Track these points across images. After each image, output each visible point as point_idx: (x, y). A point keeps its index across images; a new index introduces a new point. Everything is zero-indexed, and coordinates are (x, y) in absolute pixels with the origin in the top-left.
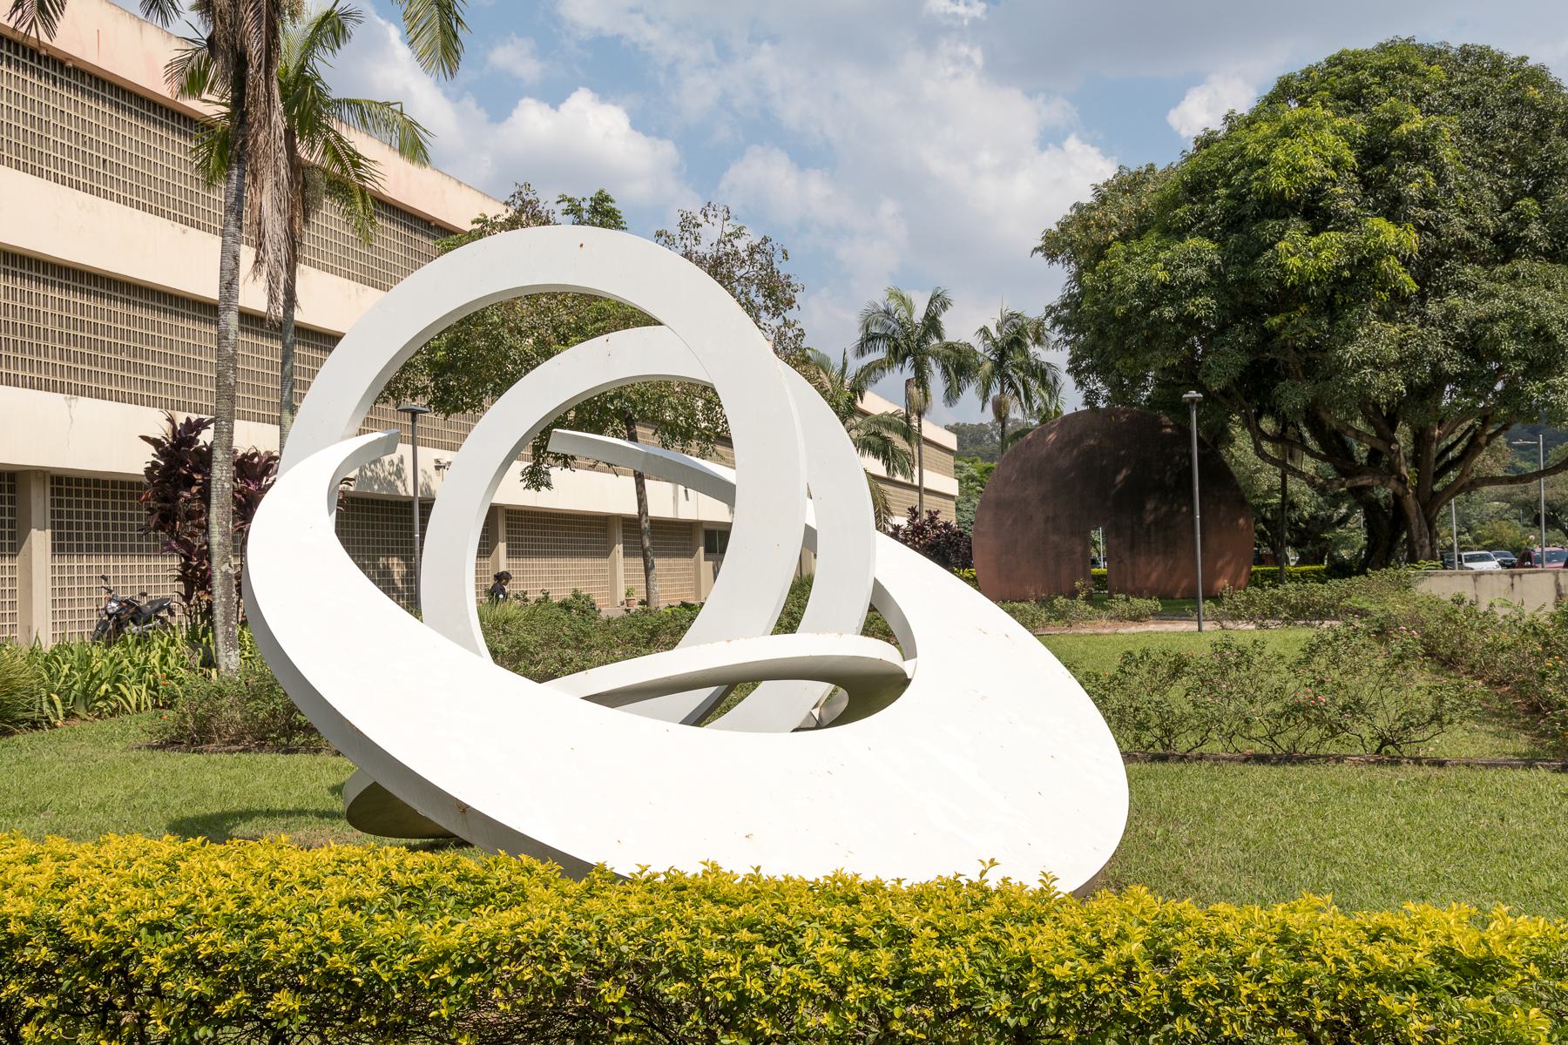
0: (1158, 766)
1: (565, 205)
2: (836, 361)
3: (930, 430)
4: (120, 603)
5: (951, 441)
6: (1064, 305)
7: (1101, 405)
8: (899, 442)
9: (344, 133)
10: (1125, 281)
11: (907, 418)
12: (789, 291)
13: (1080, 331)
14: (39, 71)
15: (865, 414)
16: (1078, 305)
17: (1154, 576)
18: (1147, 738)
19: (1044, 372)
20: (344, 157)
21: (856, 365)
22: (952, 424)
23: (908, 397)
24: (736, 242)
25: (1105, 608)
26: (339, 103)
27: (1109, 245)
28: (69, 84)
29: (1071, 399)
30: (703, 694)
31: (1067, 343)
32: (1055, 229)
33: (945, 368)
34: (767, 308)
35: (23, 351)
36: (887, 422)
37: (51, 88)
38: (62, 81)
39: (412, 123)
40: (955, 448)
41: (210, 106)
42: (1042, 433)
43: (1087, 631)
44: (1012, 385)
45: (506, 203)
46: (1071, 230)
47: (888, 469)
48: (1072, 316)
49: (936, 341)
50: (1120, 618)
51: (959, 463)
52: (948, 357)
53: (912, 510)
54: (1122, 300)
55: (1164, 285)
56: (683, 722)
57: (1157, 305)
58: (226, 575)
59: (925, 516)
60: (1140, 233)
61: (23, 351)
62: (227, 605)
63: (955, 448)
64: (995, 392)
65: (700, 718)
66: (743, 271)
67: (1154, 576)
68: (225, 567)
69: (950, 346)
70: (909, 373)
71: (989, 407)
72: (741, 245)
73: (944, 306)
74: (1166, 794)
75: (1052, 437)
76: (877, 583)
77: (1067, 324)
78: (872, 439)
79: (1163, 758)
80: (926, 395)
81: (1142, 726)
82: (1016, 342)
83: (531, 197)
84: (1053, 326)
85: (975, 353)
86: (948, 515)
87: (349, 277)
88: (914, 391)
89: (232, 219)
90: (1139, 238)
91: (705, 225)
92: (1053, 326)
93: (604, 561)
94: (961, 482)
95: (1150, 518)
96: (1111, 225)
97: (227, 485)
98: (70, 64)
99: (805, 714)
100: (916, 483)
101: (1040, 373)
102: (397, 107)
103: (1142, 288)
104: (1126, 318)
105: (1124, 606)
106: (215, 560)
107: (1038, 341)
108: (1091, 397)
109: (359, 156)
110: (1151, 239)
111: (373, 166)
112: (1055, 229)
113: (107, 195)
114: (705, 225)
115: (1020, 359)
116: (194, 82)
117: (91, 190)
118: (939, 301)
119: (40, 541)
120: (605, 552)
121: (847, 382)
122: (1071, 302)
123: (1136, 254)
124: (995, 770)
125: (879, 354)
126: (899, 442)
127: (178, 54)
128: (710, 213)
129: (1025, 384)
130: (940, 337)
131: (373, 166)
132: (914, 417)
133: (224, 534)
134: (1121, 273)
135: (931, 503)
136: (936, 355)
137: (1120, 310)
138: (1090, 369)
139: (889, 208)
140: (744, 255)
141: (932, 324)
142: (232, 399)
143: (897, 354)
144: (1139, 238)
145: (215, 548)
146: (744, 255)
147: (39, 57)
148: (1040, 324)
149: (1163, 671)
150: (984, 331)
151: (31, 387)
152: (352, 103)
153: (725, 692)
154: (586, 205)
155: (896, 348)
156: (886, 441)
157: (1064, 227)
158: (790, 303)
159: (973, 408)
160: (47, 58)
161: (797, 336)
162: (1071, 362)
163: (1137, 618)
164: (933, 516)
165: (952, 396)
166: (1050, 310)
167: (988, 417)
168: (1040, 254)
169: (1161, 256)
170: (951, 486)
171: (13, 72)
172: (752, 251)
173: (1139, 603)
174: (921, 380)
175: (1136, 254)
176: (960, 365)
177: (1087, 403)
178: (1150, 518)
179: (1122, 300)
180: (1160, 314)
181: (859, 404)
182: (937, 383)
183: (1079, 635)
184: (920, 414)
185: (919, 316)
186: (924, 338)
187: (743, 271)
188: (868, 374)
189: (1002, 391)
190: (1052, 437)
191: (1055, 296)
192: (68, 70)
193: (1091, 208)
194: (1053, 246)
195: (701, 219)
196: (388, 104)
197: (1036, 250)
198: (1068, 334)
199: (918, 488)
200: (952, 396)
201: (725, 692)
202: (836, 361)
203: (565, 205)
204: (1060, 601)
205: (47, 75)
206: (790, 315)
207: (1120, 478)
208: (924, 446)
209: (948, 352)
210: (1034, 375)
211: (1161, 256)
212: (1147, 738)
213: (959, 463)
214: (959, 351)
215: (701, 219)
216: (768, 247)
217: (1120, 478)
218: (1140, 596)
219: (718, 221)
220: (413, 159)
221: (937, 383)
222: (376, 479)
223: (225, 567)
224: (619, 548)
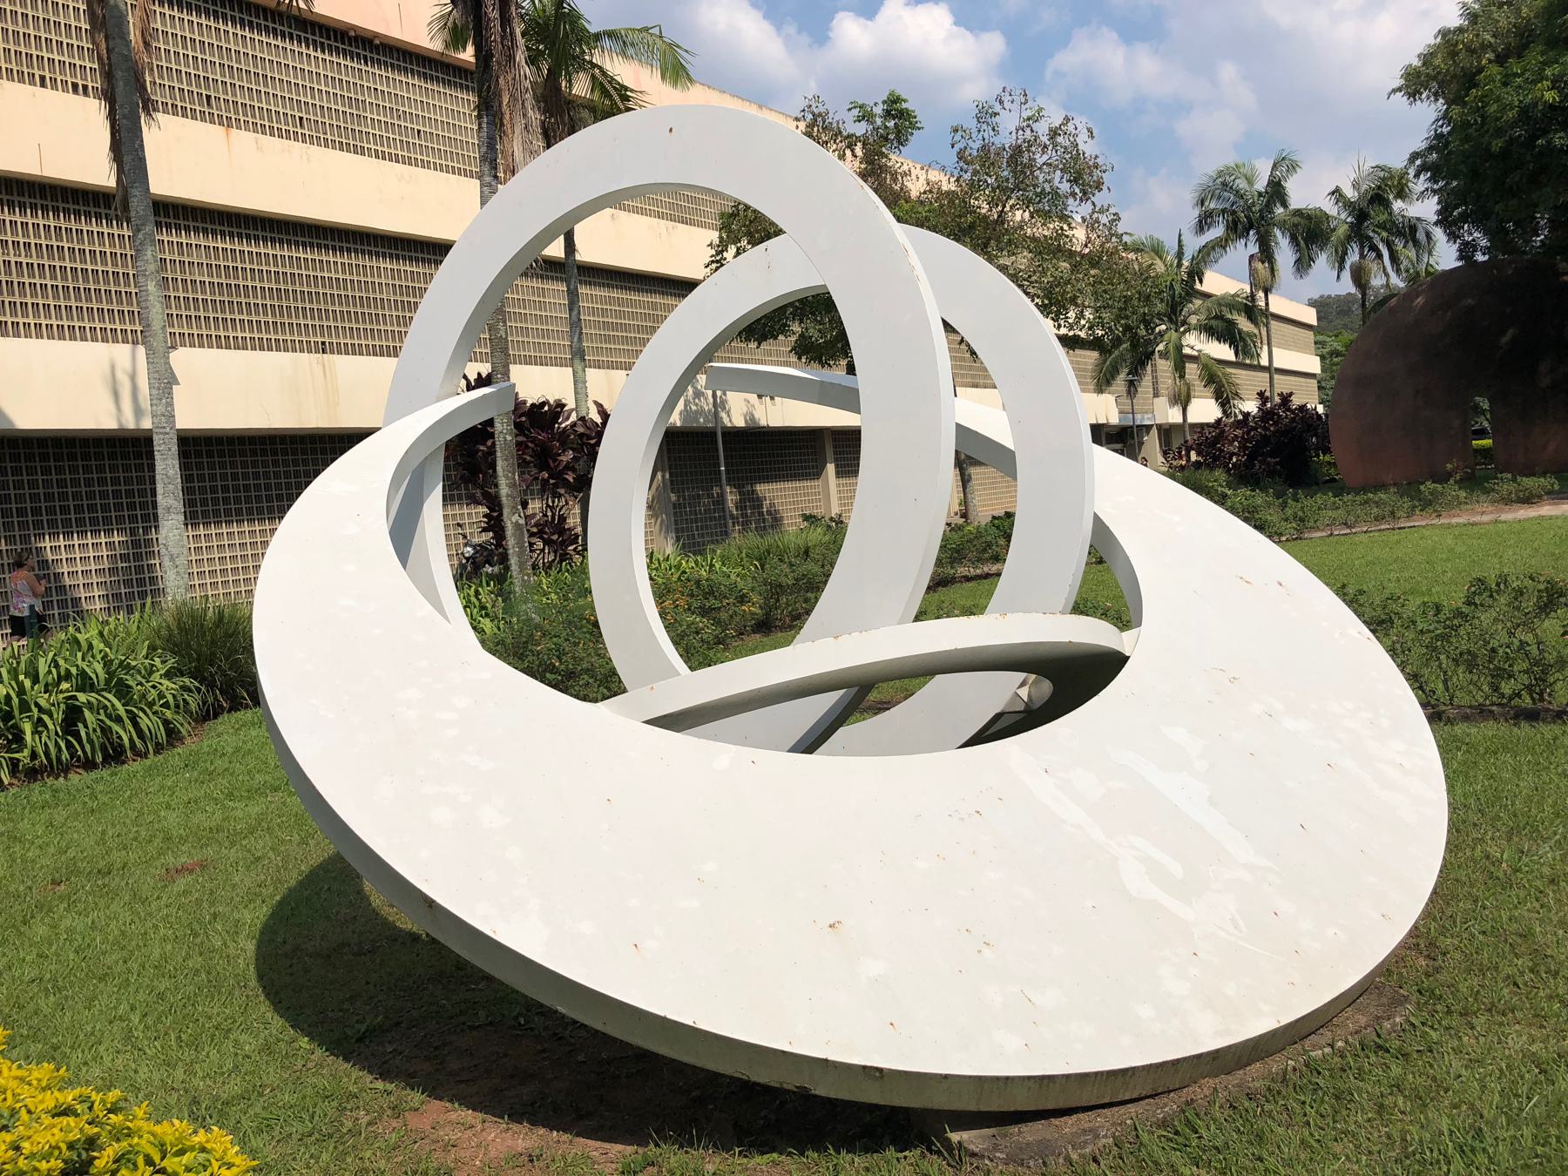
0: (1525, 730)
1: (856, 112)
2: (1171, 246)
3: (1278, 304)
4: (474, 547)
5: (1310, 316)
6: (1430, 149)
7: (1480, 258)
8: (1244, 324)
9: (608, 66)
10: (1503, 109)
11: (1252, 297)
12: (1097, 173)
13: (1451, 176)
14: (351, 53)
15: (1207, 296)
16: (1447, 144)
17: (1552, 447)
18: (1507, 688)
19: (1413, 229)
20: (613, 92)
21: (1193, 244)
22: (1316, 296)
23: (1253, 273)
24: (1035, 126)
25: (1487, 492)
26: (597, 37)
27: (1480, 70)
28: (379, 61)
29: (1445, 256)
30: (828, 700)
31: (1435, 192)
32: (1416, 62)
33: (1294, 239)
34: (1073, 194)
35: (364, 321)
36: (1230, 303)
37: (364, 68)
38: (372, 59)
39: (672, 46)
40: (1315, 323)
41: (468, 55)
42: (1409, 295)
43: (1460, 520)
44: (1374, 248)
45: (797, 119)
46: (1437, 61)
47: (1236, 354)
48: (1444, 160)
49: (1279, 210)
50: (1508, 501)
51: (1320, 338)
52: (1296, 225)
53: (1261, 394)
54: (1499, 132)
55: (1552, 107)
56: (793, 750)
57: (1545, 132)
58: (517, 525)
59: (1277, 400)
60: (1520, 51)
61: (343, 320)
62: (520, 554)
63: (1315, 323)
64: (1353, 257)
65: (811, 743)
66: (1045, 157)
67: (1552, 447)
68: (515, 518)
69: (1298, 213)
70: (1254, 248)
71: (1346, 274)
72: (1042, 128)
73: (1293, 167)
74: (1528, 781)
75: (1420, 300)
76: (1098, 523)
77: (1435, 171)
78: (1214, 323)
79: (1532, 716)
80: (1272, 270)
81: (1500, 674)
82: (1378, 198)
83: (822, 109)
84: (1417, 176)
85: (1327, 217)
86: (1309, 398)
87: (660, 216)
88: (1259, 266)
89: (486, 169)
90: (1520, 56)
91: (1002, 112)
92: (1417, 176)
93: (852, 480)
94: (1323, 358)
95: (1545, 382)
96: (1485, 47)
97: (509, 438)
98: (352, 34)
99: (1008, 695)
100: (1264, 362)
101: (1410, 231)
102: (656, 31)
103: (1525, 113)
104: (1505, 153)
105: (1512, 487)
106: (506, 512)
107: (1402, 194)
108: (1466, 251)
109: (626, 89)
110: (1534, 57)
111: (640, 96)
112: (1416, 62)
113: (425, 165)
114: (1002, 112)
115: (1383, 217)
116: (456, 38)
117: (409, 161)
118: (1285, 164)
119: (831, 468)
120: (816, 472)
121: (1186, 263)
122: (1439, 142)
123: (1516, 75)
124: (1230, 805)
125: (1217, 231)
126: (1244, 324)
127: (438, 9)
128: (1006, 98)
129: (1389, 245)
130: (1285, 205)
131: (640, 96)
132: (1261, 294)
133: (513, 485)
134: (1498, 99)
135: (1283, 384)
136: (1282, 225)
137: (1497, 145)
138: (1464, 218)
139: (1228, 72)
140: (1045, 139)
141: (1276, 191)
142: (505, 351)
143: (1237, 229)
144: (1520, 56)
145: (504, 500)
146: (1045, 139)
147: (350, 38)
148: (1403, 175)
149: (1529, 604)
150: (1337, 192)
151: (375, 354)
152: (611, 34)
153: (864, 695)
154: (878, 110)
155: (1235, 223)
156: (1232, 324)
157: (1427, 58)
158: (1099, 185)
159: (1328, 279)
160: (356, 38)
161: (1112, 222)
162: (1439, 213)
163: (1528, 500)
164: (1286, 399)
165: (1303, 264)
166: (1414, 157)
167: (1346, 286)
168: (1399, 94)
169: (1548, 72)
170: (1311, 363)
171: (229, 28)
172: (1054, 133)
173: (1528, 482)
174: (1266, 254)
175: (1516, 75)
176: (1310, 233)
177: (1460, 258)
178: (1545, 382)
179: (1499, 132)
180: (1549, 143)
181: (1198, 286)
182: (1285, 254)
183: (1449, 526)
184: (1267, 291)
185: (1261, 184)
186: (1268, 207)
187: (1045, 157)
188: (1206, 255)
189: (1362, 256)
190: (1420, 300)
191: (1419, 143)
192: (377, 47)
193: (1460, 30)
194: (1415, 83)
195: (997, 108)
196: (646, 29)
197: (1394, 91)
198: (1436, 182)
199: (1267, 369)
200: (1303, 264)
201: (864, 695)
202: (1171, 246)
203: (856, 112)
204: (1428, 486)
205: (358, 55)
206: (1100, 198)
207: (1505, 339)
208: (1273, 323)
209: (1296, 220)
210: (1400, 234)
211: (1548, 72)
212: (1507, 688)
213: (1320, 338)
214: (1309, 217)
215: (997, 108)
216: (1070, 127)
217: (1505, 339)
218: (1532, 474)
219: (1015, 106)
220: (675, 83)
221: (1285, 254)
222: (701, 412)
223: (515, 518)
224: (831, 468)
